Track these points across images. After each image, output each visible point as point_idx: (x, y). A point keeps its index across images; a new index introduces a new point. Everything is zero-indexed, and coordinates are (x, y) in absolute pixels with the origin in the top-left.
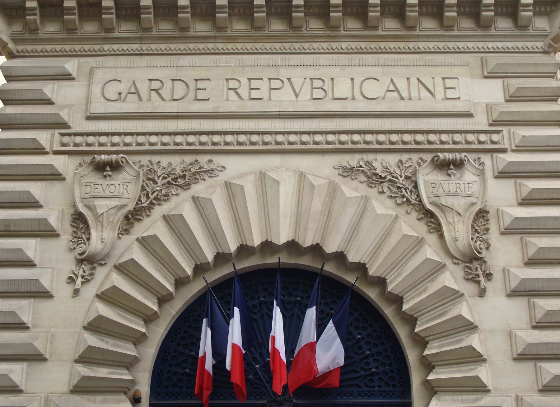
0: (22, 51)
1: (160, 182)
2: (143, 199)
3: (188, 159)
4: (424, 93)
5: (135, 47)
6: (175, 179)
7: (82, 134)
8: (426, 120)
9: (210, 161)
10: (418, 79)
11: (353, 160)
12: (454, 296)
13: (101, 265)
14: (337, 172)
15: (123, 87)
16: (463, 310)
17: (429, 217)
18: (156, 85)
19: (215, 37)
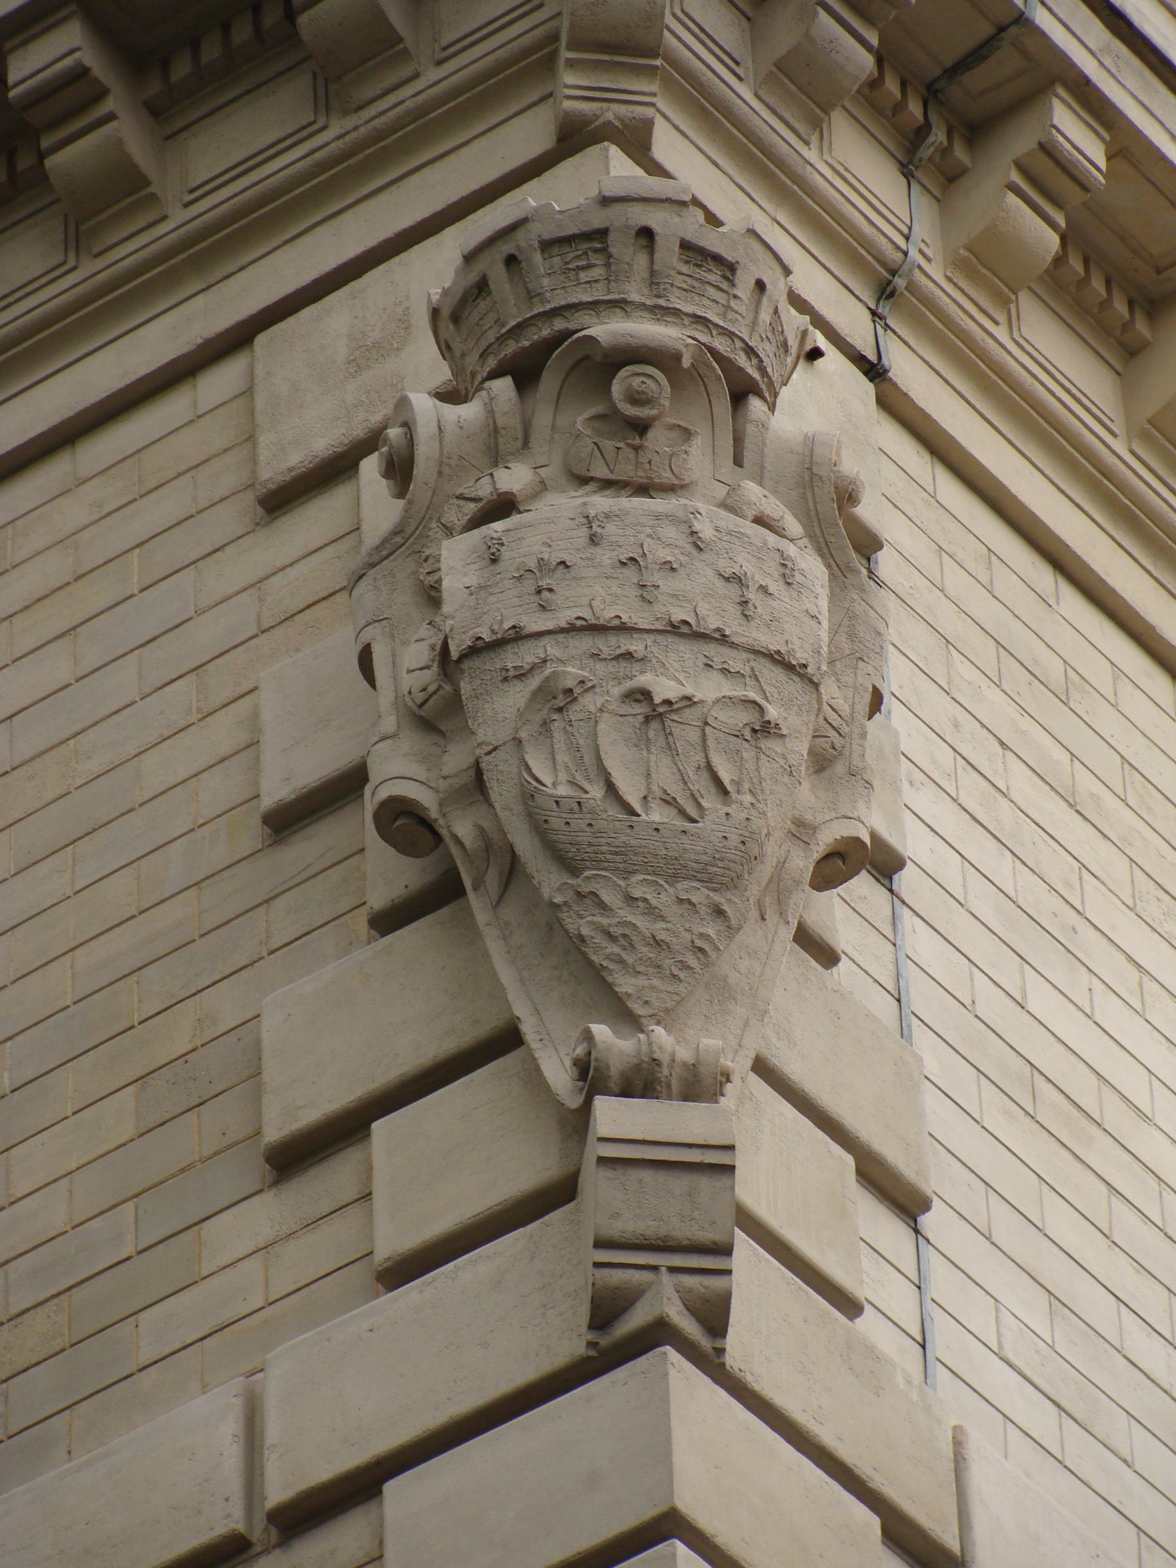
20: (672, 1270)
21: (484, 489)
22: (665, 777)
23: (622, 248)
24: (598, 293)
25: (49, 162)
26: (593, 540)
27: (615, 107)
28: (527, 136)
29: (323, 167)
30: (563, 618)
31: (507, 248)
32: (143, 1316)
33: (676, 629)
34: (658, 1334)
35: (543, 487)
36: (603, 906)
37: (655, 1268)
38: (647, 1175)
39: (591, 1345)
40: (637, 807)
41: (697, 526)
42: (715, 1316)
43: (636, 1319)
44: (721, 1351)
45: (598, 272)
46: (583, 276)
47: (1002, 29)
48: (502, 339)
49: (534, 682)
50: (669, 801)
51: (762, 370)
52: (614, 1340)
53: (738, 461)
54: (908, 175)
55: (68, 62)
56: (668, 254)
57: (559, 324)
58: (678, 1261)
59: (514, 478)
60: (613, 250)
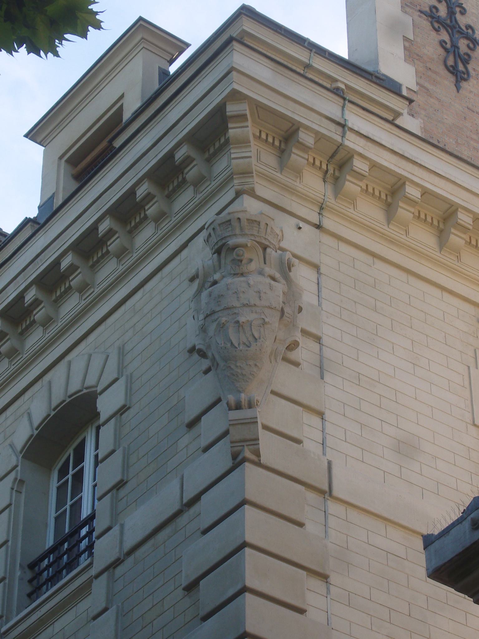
20: (247, 445)
21: (211, 280)
22: (243, 339)
23: (235, 223)
24: (230, 233)
25: (147, 213)
26: (228, 289)
27: (246, 186)
28: (231, 194)
29: (196, 206)
30: (222, 307)
31: (212, 226)
32: (169, 462)
33: (245, 305)
34: (244, 460)
35: (223, 277)
36: (232, 369)
37: (243, 446)
38: (239, 426)
39: (233, 463)
40: (237, 346)
41: (249, 282)
42: (257, 453)
43: (240, 457)
44: (260, 460)
45: (230, 229)
46: (228, 230)
47: (339, 147)
48: (214, 246)
49: (217, 322)
50: (244, 344)
51: (270, 242)
52: (237, 461)
53: (265, 263)
54: (325, 181)
55: (146, 192)
56: (244, 223)
57: (224, 241)
58: (248, 443)
59: (217, 276)
60: (232, 224)
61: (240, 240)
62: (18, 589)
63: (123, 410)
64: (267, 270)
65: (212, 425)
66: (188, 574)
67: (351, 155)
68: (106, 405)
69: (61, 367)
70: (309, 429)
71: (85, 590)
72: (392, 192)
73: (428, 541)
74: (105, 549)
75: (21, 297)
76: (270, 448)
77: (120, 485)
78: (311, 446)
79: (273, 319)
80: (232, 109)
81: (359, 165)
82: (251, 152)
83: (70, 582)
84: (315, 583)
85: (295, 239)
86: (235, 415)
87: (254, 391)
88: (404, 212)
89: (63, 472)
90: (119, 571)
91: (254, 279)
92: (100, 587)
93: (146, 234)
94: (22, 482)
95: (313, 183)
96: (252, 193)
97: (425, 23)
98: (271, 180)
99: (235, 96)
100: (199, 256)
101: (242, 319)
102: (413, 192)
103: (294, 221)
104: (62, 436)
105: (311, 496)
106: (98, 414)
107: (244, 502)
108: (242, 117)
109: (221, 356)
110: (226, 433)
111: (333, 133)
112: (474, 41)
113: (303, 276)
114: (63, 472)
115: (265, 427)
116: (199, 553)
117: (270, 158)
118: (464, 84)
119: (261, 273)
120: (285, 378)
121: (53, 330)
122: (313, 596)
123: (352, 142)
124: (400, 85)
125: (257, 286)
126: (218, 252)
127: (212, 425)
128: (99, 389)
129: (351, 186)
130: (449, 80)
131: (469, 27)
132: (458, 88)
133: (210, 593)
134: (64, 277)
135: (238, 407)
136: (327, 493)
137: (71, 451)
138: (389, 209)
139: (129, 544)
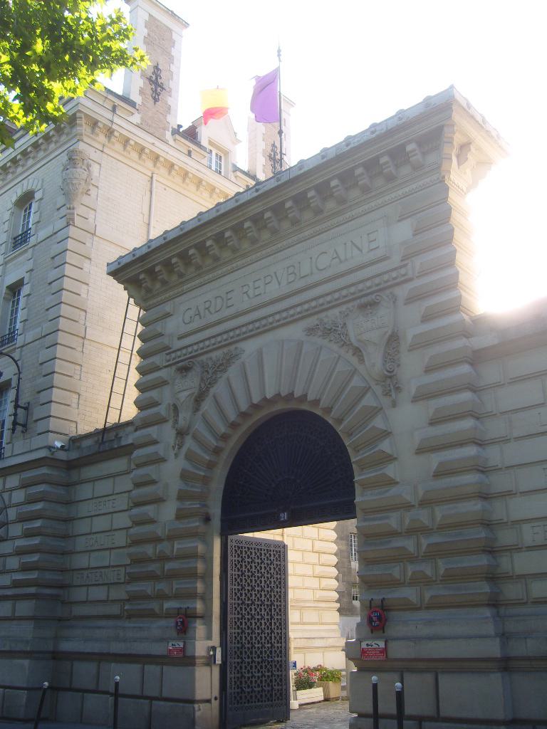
0: (423, 185)
1: (210, 371)
2: (203, 386)
3: (225, 350)
4: (356, 252)
5: (197, 282)
6: (218, 368)
7: (178, 350)
8: (228, 323)
9: (236, 348)
10: (352, 242)
11: (312, 321)
12: (376, 411)
13: (187, 435)
14: (305, 333)
15: (191, 313)
16: (378, 423)
17: (357, 352)
18: (291, 270)
19: (199, 275)
52: (68, 225)
61: (75, 157)
62: (10, 245)
63: (41, 199)
64: (83, 167)
65: (63, 211)
66: (52, 255)
67: (114, 131)
68: (38, 196)
69: (26, 180)
70: (91, 215)
71: (26, 251)
72: (126, 142)
73: (108, 264)
74: (32, 241)
75: (16, 157)
76: (77, 220)
77: (38, 222)
78: (91, 220)
79: (83, 182)
80: (78, 115)
81: (116, 134)
82: (84, 128)
83: (24, 247)
84: (87, 261)
85: (92, 154)
86: (68, 211)
87: (75, 204)
88: (129, 148)
89: (25, 211)
90: (36, 247)
91: (78, 170)
92: (29, 254)
93: (52, 146)
94: (13, 213)
95: (102, 138)
96: (82, 141)
97: (147, 82)
98: (88, 136)
99: (79, 111)
100: (64, 158)
101: (74, 182)
102: (132, 143)
103: (94, 150)
104: (25, 201)
105: (89, 235)
106: (34, 198)
107: (69, 237)
108: (81, 118)
109: (68, 192)
110: (66, 216)
111: (109, 124)
112: (163, 88)
113: (95, 168)
114: (25, 211)
115: (78, 215)
116: (56, 249)
117: (89, 130)
118: (157, 103)
119: (81, 168)
120: (85, 199)
121: (25, 168)
122: (86, 265)
123: (114, 127)
124: (136, 103)
125: (80, 172)
126: (70, 159)
127: (63, 211)
128: (37, 190)
129: (113, 139)
130: (152, 101)
131: (162, 83)
132: (155, 104)
133: (58, 261)
134: (28, 153)
135: (70, 209)
136: (94, 234)
137: (28, 205)
138: (125, 146)
139: (39, 240)
